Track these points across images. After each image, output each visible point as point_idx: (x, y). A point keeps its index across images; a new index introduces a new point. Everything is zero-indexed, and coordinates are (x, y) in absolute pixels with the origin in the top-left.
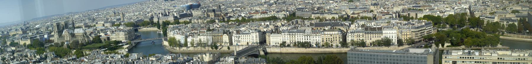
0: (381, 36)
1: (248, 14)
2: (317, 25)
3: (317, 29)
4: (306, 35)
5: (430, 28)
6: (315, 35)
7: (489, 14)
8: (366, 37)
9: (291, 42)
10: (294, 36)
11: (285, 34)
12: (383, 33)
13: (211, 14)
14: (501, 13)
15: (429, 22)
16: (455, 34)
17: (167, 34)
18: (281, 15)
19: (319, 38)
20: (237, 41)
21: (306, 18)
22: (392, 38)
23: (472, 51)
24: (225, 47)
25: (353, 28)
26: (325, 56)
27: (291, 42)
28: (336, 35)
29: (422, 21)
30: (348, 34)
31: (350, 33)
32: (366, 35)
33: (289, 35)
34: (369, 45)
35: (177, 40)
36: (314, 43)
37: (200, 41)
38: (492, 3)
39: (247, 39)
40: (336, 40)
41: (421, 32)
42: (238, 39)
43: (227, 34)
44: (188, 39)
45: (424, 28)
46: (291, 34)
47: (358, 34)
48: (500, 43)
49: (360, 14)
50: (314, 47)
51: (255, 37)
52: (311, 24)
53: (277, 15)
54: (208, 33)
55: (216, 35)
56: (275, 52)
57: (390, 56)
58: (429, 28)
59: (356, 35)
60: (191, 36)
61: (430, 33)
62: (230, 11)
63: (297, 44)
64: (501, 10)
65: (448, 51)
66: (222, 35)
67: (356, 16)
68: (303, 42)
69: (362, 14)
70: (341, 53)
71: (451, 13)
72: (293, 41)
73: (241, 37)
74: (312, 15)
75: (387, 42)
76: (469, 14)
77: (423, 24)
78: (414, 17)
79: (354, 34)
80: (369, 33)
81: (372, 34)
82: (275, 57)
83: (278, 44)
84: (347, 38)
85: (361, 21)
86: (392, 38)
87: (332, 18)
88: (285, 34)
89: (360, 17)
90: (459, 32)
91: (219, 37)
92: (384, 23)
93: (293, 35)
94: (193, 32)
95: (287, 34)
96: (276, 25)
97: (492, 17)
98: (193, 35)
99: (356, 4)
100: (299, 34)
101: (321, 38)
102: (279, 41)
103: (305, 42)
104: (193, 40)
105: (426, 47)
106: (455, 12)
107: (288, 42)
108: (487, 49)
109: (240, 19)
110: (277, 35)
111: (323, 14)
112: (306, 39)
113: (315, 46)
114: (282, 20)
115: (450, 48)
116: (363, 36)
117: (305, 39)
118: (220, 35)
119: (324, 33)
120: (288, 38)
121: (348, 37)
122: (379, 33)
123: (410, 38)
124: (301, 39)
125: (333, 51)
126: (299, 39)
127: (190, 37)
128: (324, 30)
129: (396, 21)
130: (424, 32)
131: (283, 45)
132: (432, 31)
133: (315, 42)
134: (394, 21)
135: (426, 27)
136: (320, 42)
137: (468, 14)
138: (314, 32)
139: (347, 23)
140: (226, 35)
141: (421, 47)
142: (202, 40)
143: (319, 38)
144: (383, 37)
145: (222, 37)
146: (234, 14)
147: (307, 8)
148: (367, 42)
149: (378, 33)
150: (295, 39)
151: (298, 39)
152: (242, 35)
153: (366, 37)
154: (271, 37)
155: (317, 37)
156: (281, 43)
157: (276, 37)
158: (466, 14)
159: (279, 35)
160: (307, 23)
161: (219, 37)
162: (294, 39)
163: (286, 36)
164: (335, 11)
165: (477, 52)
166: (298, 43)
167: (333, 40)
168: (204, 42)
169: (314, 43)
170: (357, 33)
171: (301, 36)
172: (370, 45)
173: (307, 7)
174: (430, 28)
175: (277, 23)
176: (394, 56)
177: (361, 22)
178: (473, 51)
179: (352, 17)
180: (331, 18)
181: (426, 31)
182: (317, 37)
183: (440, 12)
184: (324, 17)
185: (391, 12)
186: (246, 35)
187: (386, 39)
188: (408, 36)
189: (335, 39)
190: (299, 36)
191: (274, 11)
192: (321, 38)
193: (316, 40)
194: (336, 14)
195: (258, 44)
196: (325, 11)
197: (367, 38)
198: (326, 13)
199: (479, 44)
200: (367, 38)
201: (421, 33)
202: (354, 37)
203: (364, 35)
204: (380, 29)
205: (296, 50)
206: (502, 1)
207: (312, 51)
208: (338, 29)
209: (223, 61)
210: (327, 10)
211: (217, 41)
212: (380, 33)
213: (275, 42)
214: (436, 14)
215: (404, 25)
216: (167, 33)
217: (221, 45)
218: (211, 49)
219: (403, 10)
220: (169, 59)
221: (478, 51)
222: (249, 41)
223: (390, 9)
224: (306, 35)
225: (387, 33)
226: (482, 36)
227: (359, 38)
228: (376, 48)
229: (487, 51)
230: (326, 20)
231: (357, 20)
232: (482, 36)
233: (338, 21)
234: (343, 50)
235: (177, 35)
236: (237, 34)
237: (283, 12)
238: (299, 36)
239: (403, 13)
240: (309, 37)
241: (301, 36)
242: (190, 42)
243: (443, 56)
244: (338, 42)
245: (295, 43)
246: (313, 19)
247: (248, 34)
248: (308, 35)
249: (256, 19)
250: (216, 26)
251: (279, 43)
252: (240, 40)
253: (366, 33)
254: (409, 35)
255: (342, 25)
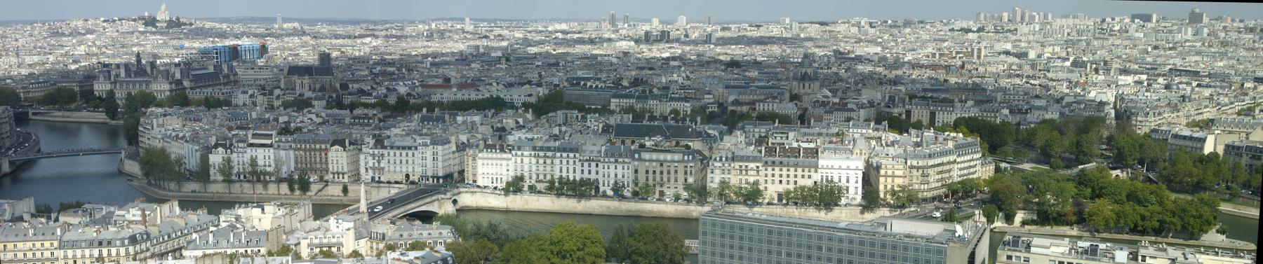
0: (812, 173)
1: (417, 87)
2: (622, 131)
3: (623, 142)
4: (586, 160)
5: (972, 160)
6: (613, 160)
7: (1188, 125)
8: (766, 176)
9: (541, 177)
10: (549, 161)
11: (522, 154)
12: (820, 166)
13: (299, 81)
14: (1225, 122)
15: (970, 140)
16: (1054, 184)
17: (140, 139)
18: (518, 95)
19: (623, 169)
20: (374, 169)
21: (593, 107)
22: (848, 181)
23: (1102, 246)
24: (333, 187)
25: (729, 145)
26: (638, 226)
27: (541, 177)
28: (676, 164)
29: (948, 135)
30: (713, 165)
31: (718, 159)
32: (766, 170)
33: (535, 156)
34: (773, 199)
35: (173, 156)
36: (608, 186)
37: (251, 165)
38: (1201, 89)
39: (407, 163)
40: (676, 180)
41: (940, 169)
42: (379, 163)
43: (344, 147)
44: (210, 155)
45: (952, 158)
46: (542, 154)
47: (744, 164)
48: (1218, 227)
49: (757, 104)
50: (609, 197)
51: (430, 158)
52: (607, 129)
53: (505, 95)
54: (280, 141)
55: (308, 146)
56: (490, 205)
57: (830, 239)
58: (969, 157)
59: (737, 167)
60: (224, 146)
61: (969, 174)
62: (362, 73)
63: (557, 184)
64: (1235, 116)
65: (1019, 237)
66: (326, 149)
67: (745, 109)
68: (574, 179)
69: (762, 105)
70: (688, 219)
71: (1048, 116)
72: (545, 175)
73: (386, 159)
74: (612, 100)
75: (828, 197)
76: (1114, 122)
77: (951, 144)
78: (926, 121)
79: (730, 165)
80: (777, 163)
81: (785, 166)
82: (484, 220)
83: (501, 182)
84: (709, 175)
85: (755, 126)
86: (848, 181)
87: (671, 112)
88: (522, 154)
89: (755, 115)
90: (1068, 180)
91: (318, 154)
92: (827, 135)
93: (548, 157)
94: (230, 135)
95: (531, 155)
96: (499, 125)
97: (1195, 135)
98: (231, 145)
99: (747, 74)
100: (565, 155)
101: (630, 171)
102: (505, 172)
103: (582, 179)
104: (229, 161)
105: (949, 218)
106: (1062, 114)
107: (499, 187)
108: (1161, 243)
109: (390, 102)
110: (499, 156)
111: (646, 98)
112: (586, 172)
113: (610, 193)
114: (520, 111)
115: (1034, 227)
116: (758, 171)
117: (582, 170)
118: (321, 148)
119: (640, 155)
120: (530, 167)
121: (712, 173)
122: (806, 167)
123: (903, 188)
124: (571, 170)
125: (665, 212)
126: (564, 170)
127: (220, 149)
128: (642, 146)
129: (864, 131)
130: (949, 171)
131: (515, 186)
132: (978, 168)
133: (612, 182)
134: (859, 131)
135: (959, 156)
136: (626, 183)
137: (1108, 122)
138: (614, 155)
139: (714, 129)
140: (340, 148)
141: (928, 218)
142: (261, 163)
143: (623, 169)
144: (817, 177)
145: (326, 154)
146: (375, 86)
147: (599, 79)
148: (769, 192)
149: (803, 167)
150: (552, 171)
151: (561, 171)
152: (392, 152)
153: (766, 176)
154: (480, 162)
155: (620, 167)
156: (510, 179)
157: (494, 162)
158: (1103, 120)
159: (505, 156)
160: (595, 123)
161: (318, 154)
162: (549, 168)
163: (526, 160)
164: (682, 91)
165: (1121, 249)
166: (559, 184)
167: (665, 179)
168: (268, 169)
169: (608, 186)
170: (740, 161)
171: (571, 162)
172: (776, 202)
173: (599, 76)
174: (972, 160)
175: (504, 121)
176: (841, 240)
177: (757, 130)
178: (1109, 244)
179: (733, 112)
180: (668, 112)
181: (956, 166)
182: (620, 167)
183: (1011, 112)
184: (648, 107)
185: (853, 103)
186: (404, 153)
187: (827, 186)
188: (899, 181)
189: (672, 176)
190: (564, 161)
191: (498, 84)
192: (630, 171)
193: (616, 176)
194: (686, 99)
195: (438, 181)
196: (651, 91)
197: (769, 178)
198: (654, 97)
199: (1140, 223)
200: (769, 178)
201: (941, 172)
202: (729, 173)
203: (760, 168)
204: (814, 153)
205: (554, 203)
206: (1243, 85)
207: (601, 207)
208: (682, 146)
209: (319, 229)
210: (659, 89)
211: (309, 166)
212: (810, 167)
213: (490, 177)
214: (997, 115)
215: (887, 145)
216: (140, 134)
217: (321, 179)
218: (289, 193)
219: (892, 99)
220: (131, 222)
221: (1125, 247)
222: (410, 170)
223: (852, 94)
224: (586, 160)
225: (832, 168)
226: (1153, 199)
227: (746, 177)
228: (795, 212)
229: (1160, 250)
230: (652, 118)
231: (745, 122)
232: (1153, 199)
233: (688, 123)
234: (693, 211)
235: (173, 143)
236: (376, 148)
237: (525, 87)
238: (564, 161)
239: (889, 107)
240: (593, 164)
241: (571, 162)
242: (217, 167)
243: (999, 252)
244: (682, 187)
245: (552, 182)
246: (612, 112)
247: (410, 148)
248: (593, 160)
249: (442, 103)
250: (311, 119)
251: (505, 179)
252: (382, 165)
253: (766, 162)
254: (900, 177)
255: (698, 135)
